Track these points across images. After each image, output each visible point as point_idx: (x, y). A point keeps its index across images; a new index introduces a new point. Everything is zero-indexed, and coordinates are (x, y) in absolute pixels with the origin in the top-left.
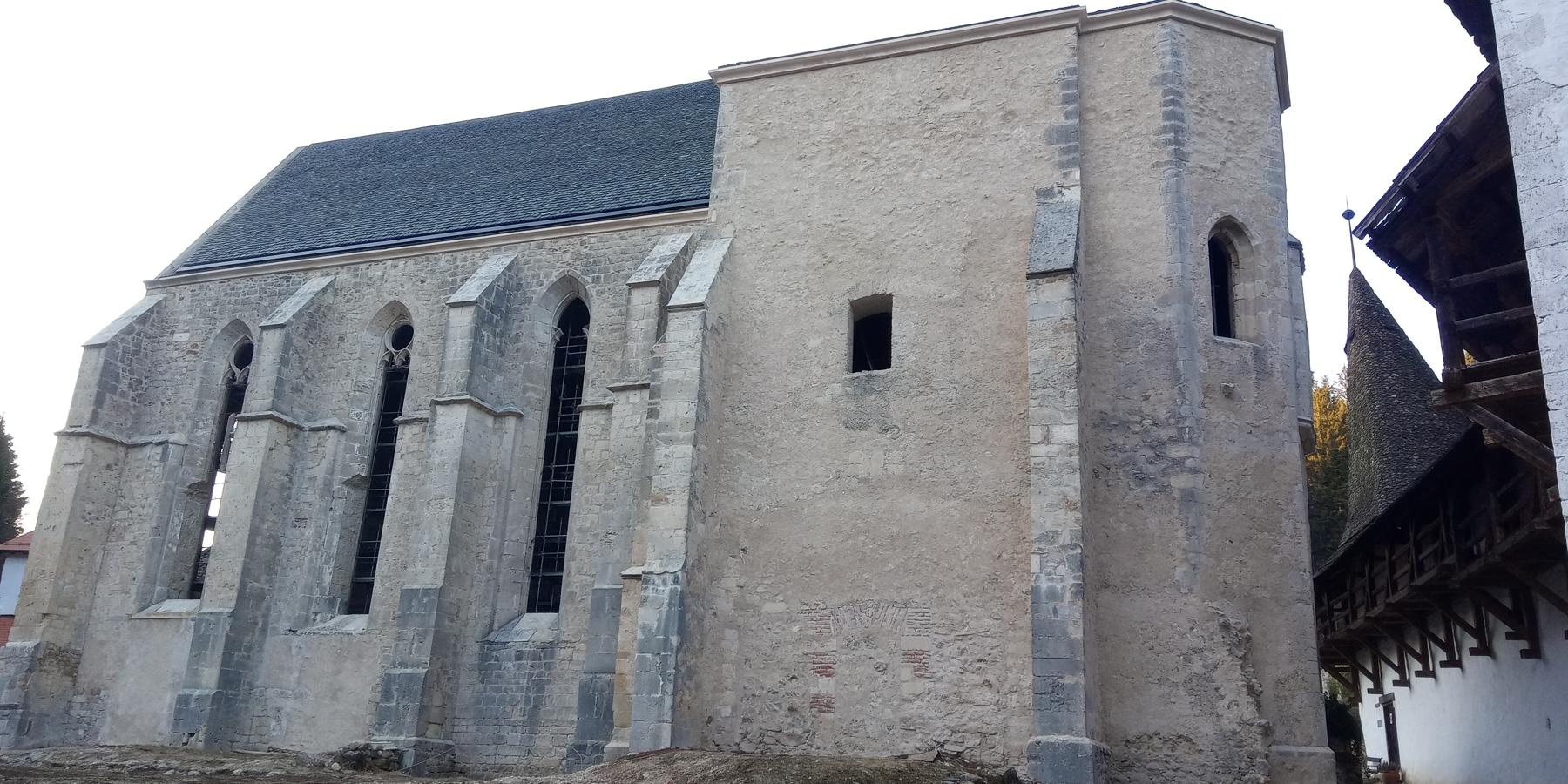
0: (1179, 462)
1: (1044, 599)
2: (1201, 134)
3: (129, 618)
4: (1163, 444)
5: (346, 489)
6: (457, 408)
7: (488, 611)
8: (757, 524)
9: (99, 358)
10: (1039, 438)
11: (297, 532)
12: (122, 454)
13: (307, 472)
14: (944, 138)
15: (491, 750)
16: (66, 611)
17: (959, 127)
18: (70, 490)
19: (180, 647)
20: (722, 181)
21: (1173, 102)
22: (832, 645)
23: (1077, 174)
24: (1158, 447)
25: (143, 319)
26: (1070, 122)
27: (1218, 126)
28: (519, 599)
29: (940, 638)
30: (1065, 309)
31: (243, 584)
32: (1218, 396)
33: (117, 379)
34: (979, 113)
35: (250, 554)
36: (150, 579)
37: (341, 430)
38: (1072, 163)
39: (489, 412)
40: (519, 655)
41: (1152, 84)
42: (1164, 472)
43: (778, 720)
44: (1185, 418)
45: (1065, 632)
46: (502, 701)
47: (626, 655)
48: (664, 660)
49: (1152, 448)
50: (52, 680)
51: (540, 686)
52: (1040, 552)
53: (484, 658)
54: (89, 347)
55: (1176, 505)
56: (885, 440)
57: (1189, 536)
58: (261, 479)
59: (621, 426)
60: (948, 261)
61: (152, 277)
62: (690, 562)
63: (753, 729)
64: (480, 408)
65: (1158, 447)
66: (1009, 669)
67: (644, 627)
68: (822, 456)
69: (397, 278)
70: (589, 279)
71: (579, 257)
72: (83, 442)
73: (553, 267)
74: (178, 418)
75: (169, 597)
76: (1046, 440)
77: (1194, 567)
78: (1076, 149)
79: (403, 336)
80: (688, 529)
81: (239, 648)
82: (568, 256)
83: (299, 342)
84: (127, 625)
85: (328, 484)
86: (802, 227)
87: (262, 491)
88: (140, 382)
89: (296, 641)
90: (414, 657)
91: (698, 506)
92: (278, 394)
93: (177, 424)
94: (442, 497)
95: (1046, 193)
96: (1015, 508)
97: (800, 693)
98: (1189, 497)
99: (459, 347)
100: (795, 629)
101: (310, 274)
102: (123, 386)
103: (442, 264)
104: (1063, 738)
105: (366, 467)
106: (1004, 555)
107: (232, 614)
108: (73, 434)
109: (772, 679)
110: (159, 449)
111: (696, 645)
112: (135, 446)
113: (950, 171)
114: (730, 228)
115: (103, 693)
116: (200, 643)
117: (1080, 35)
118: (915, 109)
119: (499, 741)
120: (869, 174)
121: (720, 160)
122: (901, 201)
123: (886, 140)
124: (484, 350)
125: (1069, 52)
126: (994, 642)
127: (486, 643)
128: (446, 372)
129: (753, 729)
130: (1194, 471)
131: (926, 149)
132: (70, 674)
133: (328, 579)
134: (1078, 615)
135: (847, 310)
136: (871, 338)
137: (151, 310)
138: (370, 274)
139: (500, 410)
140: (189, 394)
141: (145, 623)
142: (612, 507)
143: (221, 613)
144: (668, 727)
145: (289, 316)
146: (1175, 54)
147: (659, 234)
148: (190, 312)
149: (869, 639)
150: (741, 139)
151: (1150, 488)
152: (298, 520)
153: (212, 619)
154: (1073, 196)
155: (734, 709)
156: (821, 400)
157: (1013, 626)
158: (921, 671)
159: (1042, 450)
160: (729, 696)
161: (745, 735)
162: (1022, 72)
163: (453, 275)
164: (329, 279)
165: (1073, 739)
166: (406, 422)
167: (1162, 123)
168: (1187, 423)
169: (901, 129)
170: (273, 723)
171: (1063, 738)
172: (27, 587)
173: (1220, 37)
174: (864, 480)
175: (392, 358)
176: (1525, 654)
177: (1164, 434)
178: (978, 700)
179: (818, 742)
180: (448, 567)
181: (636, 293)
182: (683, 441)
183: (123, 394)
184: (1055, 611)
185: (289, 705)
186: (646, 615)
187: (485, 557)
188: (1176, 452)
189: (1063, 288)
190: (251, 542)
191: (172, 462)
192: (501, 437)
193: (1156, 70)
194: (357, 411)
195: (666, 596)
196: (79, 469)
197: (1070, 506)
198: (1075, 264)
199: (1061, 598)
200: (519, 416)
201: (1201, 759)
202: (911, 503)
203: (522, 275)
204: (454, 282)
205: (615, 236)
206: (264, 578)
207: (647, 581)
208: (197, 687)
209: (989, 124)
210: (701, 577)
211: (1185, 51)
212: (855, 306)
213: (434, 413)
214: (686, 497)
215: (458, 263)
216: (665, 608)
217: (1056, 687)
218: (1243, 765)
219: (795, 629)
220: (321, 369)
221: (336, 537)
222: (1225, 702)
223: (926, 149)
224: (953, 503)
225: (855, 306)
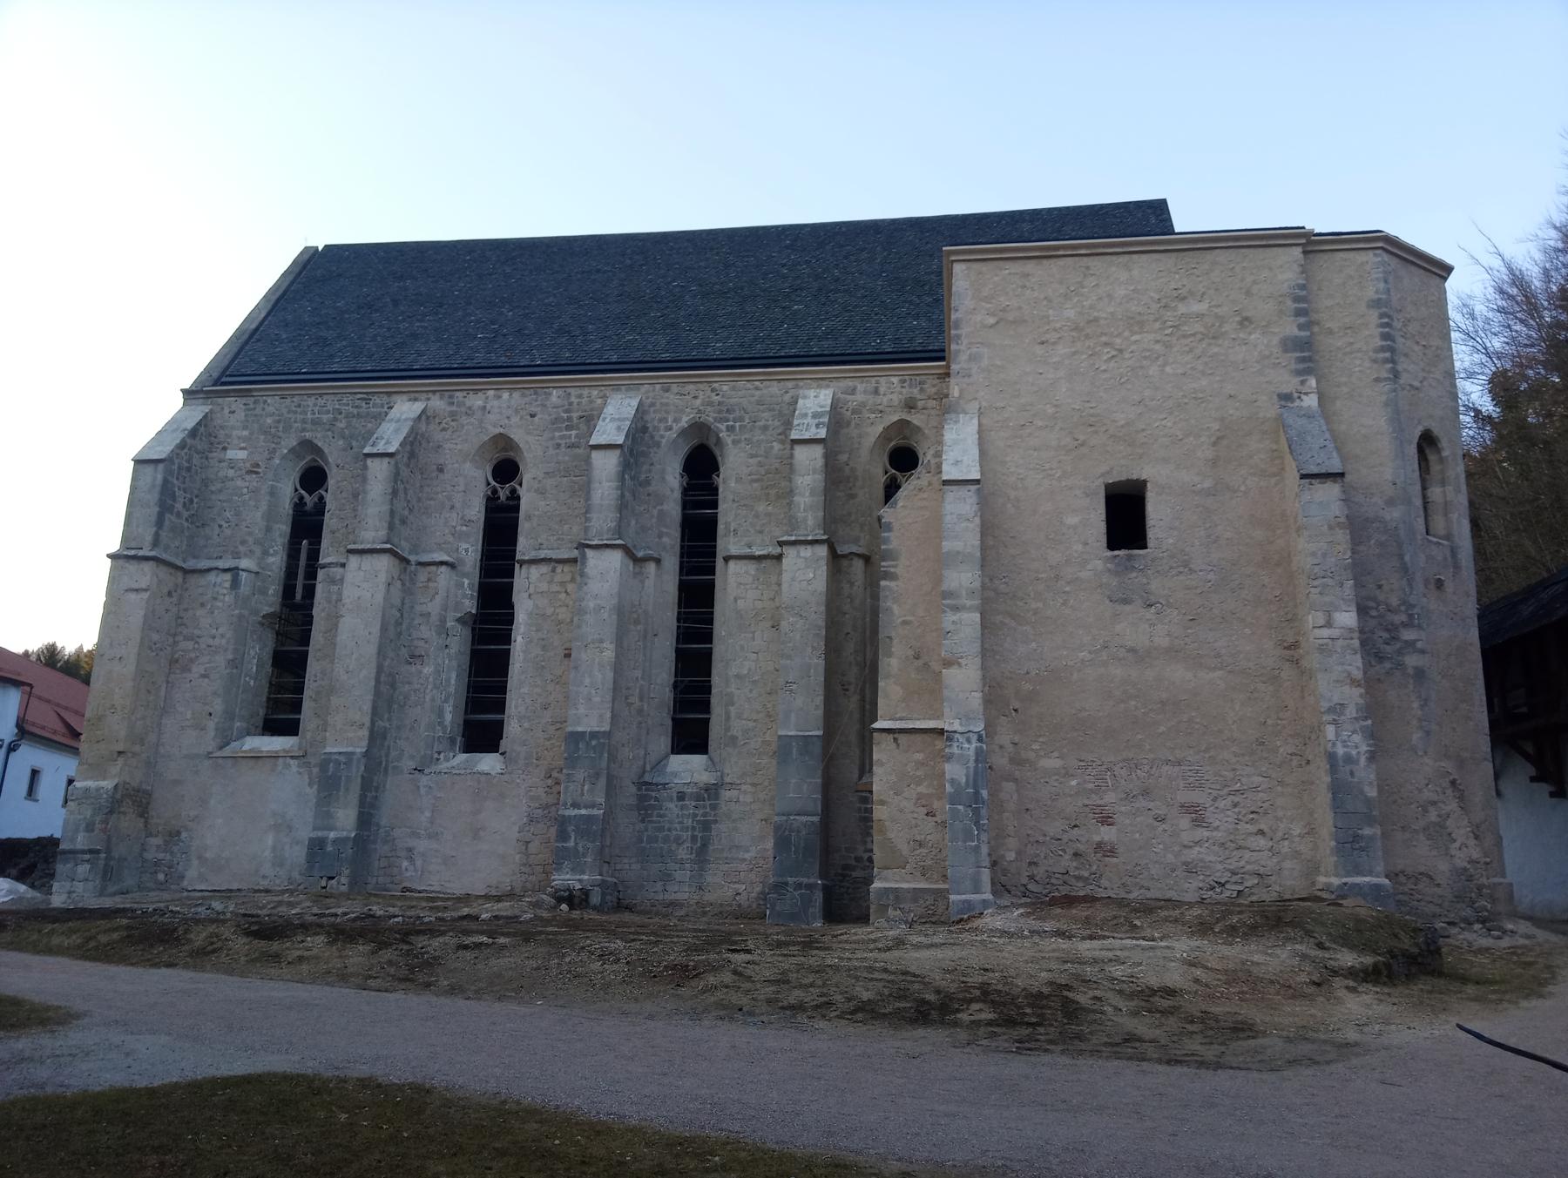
2: (1406, 355)
3: (209, 756)
6: (608, 552)
8: (1028, 687)
9: (155, 476)
10: (1322, 622)
11: (413, 669)
12: (180, 580)
13: (418, 608)
14: (1185, 336)
15: (659, 886)
16: (137, 748)
17: (1198, 327)
18: (137, 618)
20: (963, 357)
21: (1387, 325)
22: (1110, 797)
23: (1313, 382)
24: (1392, 630)
25: (193, 433)
26: (1303, 334)
27: (1416, 348)
28: (663, 741)
29: (1215, 793)
31: (373, 722)
32: (1432, 586)
33: (174, 498)
34: (1217, 316)
36: (229, 715)
37: (452, 566)
38: (1308, 372)
40: (681, 796)
42: (1400, 652)
44: (1414, 606)
45: (1362, 792)
46: (666, 840)
48: (976, 812)
49: (1388, 630)
50: (128, 822)
51: (706, 826)
52: (1335, 722)
53: (642, 798)
57: (1422, 707)
59: (793, 579)
60: (1199, 454)
63: (1039, 872)
65: (1392, 630)
66: (1281, 819)
67: (952, 781)
68: (1092, 627)
69: (501, 409)
71: (710, 404)
72: (148, 567)
73: (682, 411)
74: (243, 542)
76: (1329, 624)
77: (1428, 733)
78: (1310, 359)
82: (698, 402)
84: (207, 763)
85: (443, 621)
86: (1050, 410)
87: (384, 629)
88: (191, 501)
89: (424, 780)
90: (587, 797)
93: (242, 549)
94: (601, 641)
95: (1286, 398)
97: (1083, 840)
98: (1420, 674)
100: (1074, 783)
101: (395, 397)
102: (179, 506)
104: (1367, 879)
106: (1269, 722)
107: (366, 754)
108: (127, 557)
109: (1054, 828)
110: (228, 576)
112: (194, 571)
113: (1193, 369)
114: (974, 406)
115: (184, 835)
117: (1305, 252)
118: (1155, 306)
119: (666, 877)
120: (1112, 364)
121: (959, 337)
122: (1147, 393)
123: (1126, 334)
125: (1296, 268)
127: (642, 784)
128: (594, 515)
129: (1039, 872)
130: (1423, 652)
131: (1168, 346)
132: (141, 815)
133: (448, 717)
134: (1372, 776)
136: (1125, 516)
137: (199, 423)
138: (468, 403)
139: (640, 554)
140: (255, 517)
141: (230, 762)
142: (789, 657)
143: (353, 753)
147: (796, 387)
148: (245, 428)
149: (1146, 793)
150: (979, 318)
151: (1388, 665)
152: (412, 656)
153: (342, 759)
154: (1311, 401)
155: (1019, 853)
156: (1084, 575)
158: (1199, 822)
160: (1012, 843)
161: (1031, 878)
162: (1254, 282)
163: (567, 411)
165: (1375, 880)
166: (522, 563)
167: (1379, 343)
169: (1141, 324)
170: (405, 864)
171: (1367, 879)
173: (1413, 268)
174: (1132, 650)
175: (495, 491)
176: (1552, 795)
177: (1399, 618)
178: (1254, 846)
179: (1104, 883)
181: (798, 450)
182: (970, 609)
184: (1352, 773)
185: (421, 845)
187: (635, 699)
188: (1408, 635)
190: (378, 681)
191: (245, 589)
192: (642, 582)
193: (1370, 293)
195: (972, 753)
196: (146, 595)
197: (1354, 682)
199: (1357, 762)
200: (658, 561)
201: (1439, 891)
202: (1178, 673)
203: (647, 418)
205: (749, 385)
207: (950, 739)
209: (1227, 327)
211: (1391, 278)
212: (1108, 487)
216: (972, 764)
217: (1356, 838)
219: (1074, 783)
220: (419, 500)
221: (454, 675)
222: (1457, 845)
223: (1168, 346)
224: (1219, 673)
225: (1108, 487)
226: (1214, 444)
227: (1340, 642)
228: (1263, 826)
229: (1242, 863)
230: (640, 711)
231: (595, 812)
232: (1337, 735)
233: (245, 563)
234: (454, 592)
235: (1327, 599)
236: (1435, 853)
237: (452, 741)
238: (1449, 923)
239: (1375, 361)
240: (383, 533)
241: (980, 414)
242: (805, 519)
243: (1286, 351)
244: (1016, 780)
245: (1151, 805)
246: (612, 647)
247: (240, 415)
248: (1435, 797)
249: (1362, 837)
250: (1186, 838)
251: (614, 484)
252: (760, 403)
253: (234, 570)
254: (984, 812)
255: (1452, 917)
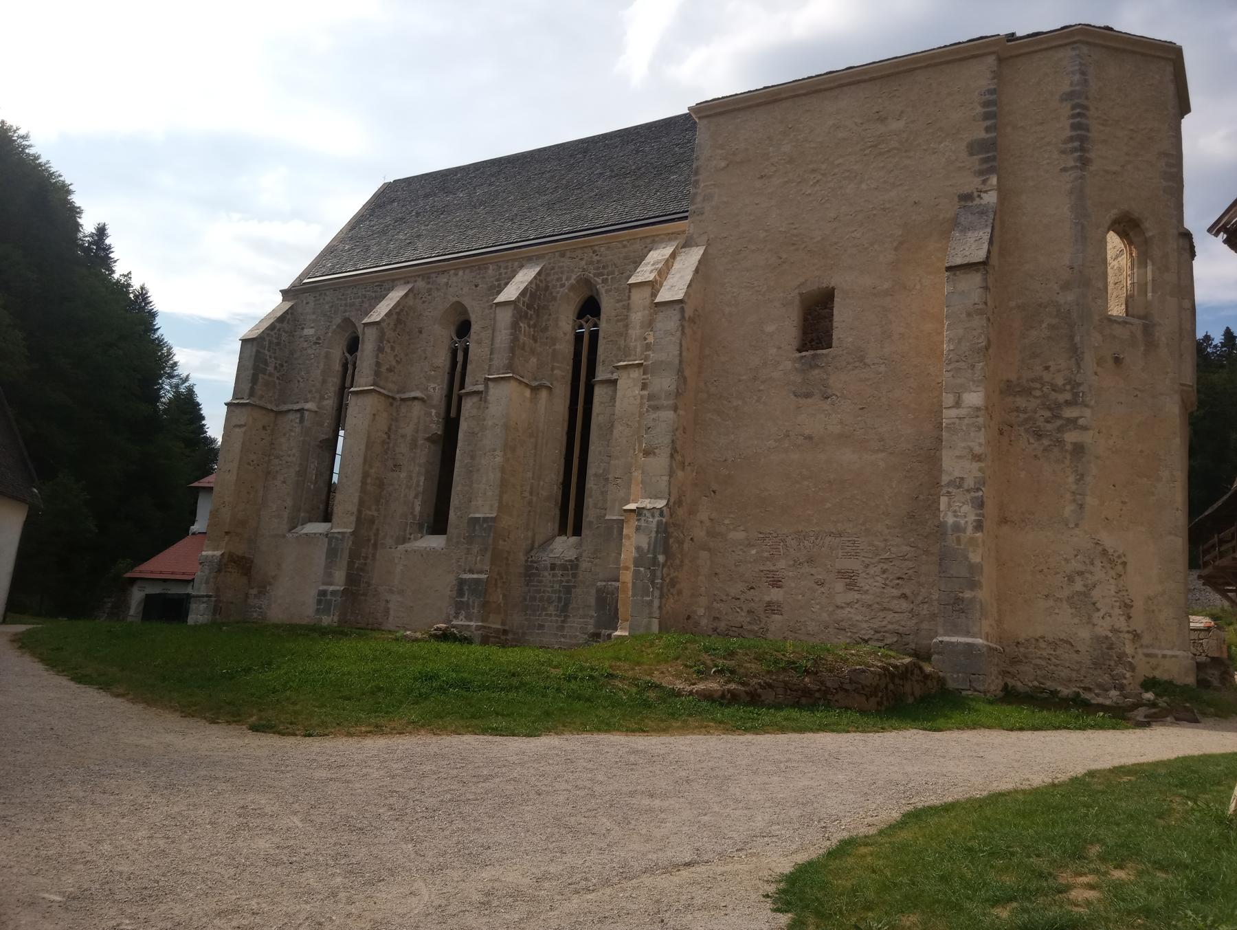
0: (1073, 422)
1: (950, 532)
4: (1059, 406)
5: (427, 444)
7: (530, 534)
9: (253, 349)
19: (319, 555)
22: (782, 564)
23: (994, 180)
24: (1055, 410)
25: (281, 319)
28: (552, 527)
29: (867, 561)
30: (976, 296)
31: (360, 512)
33: (266, 364)
35: (363, 490)
38: (991, 170)
39: (527, 385)
40: (553, 567)
41: (1062, 100)
42: (1060, 429)
43: (740, 619)
44: (1080, 384)
45: (966, 558)
46: (541, 600)
47: (627, 568)
48: (653, 573)
49: (1050, 409)
51: (568, 590)
54: (245, 342)
55: (1068, 457)
56: (826, 405)
58: (369, 437)
61: (286, 286)
62: (672, 500)
64: (521, 382)
70: (599, 281)
71: (591, 263)
74: (310, 392)
75: (310, 521)
76: (957, 404)
79: (464, 328)
80: (670, 476)
81: (359, 556)
83: (389, 334)
86: (762, 235)
87: (369, 445)
88: (282, 366)
91: (678, 458)
92: (377, 374)
93: (309, 396)
95: (967, 197)
96: (932, 458)
97: (757, 599)
99: (503, 336)
100: (754, 552)
102: (270, 369)
103: (490, 271)
105: (441, 426)
106: (921, 497)
107: (353, 533)
110: (298, 415)
111: (677, 562)
113: (885, 182)
116: (332, 554)
120: (817, 188)
124: (522, 338)
126: (910, 564)
133: (418, 509)
135: (797, 301)
136: (816, 323)
137: (286, 312)
139: (535, 384)
144: (656, 621)
145: (383, 314)
146: (1083, 73)
149: (810, 561)
151: (1046, 442)
154: (991, 198)
157: (926, 552)
158: (851, 585)
159: (953, 413)
163: (498, 280)
164: (409, 286)
167: (1068, 133)
168: (1081, 388)
172: (214, 514)
174: (810, 438)
180: (500, 502)
183: (271, 375)
186: (634, 542)
188: (1069, 413)
189: (976, 279)
190: (364, 483)
191: (307, 424)
193: (1067, 88)
194: (433, 385)
195: (654, 525)
196: (243, 429)
198: (987, 257)
204: (499, 286)
206: (374, 508)
208: (331, 584)
210: (680, 512)
213: (487, 387)
214: (668, 451)
215: (503, 271)
216: (653, 535)
217: (959, 600)
218: (1112, 663)
219: (754, 552)
221: (422, 479)
222: (1101, 613)
224: (881, 455)
226: (896, 249)
227: (966, 421)
228: (907, 591)
229: (884, 623)
230: (530, 503)
231: (484, 576)
232: (949, 505)
233: (309, 406)
234: (422, 420)
235: (959, 381)
236: (1076, 620)
237: (421, 526)
238: (1085, 689)
239: (1063, 152)
240: (371, 379)
241: (708, 245)
242: (635, 347)
243: (971, 154)
244: (709, 550)
245: (813, 571)
246: (501, 454)
247: (312, 304)
248: (1081, 568)
249: (962, 600)
250: (839, 600)
251: (509, 332)
252: (626, 258)
253: (301, 411)
254: (659, 574)
255: (1087, 683)
